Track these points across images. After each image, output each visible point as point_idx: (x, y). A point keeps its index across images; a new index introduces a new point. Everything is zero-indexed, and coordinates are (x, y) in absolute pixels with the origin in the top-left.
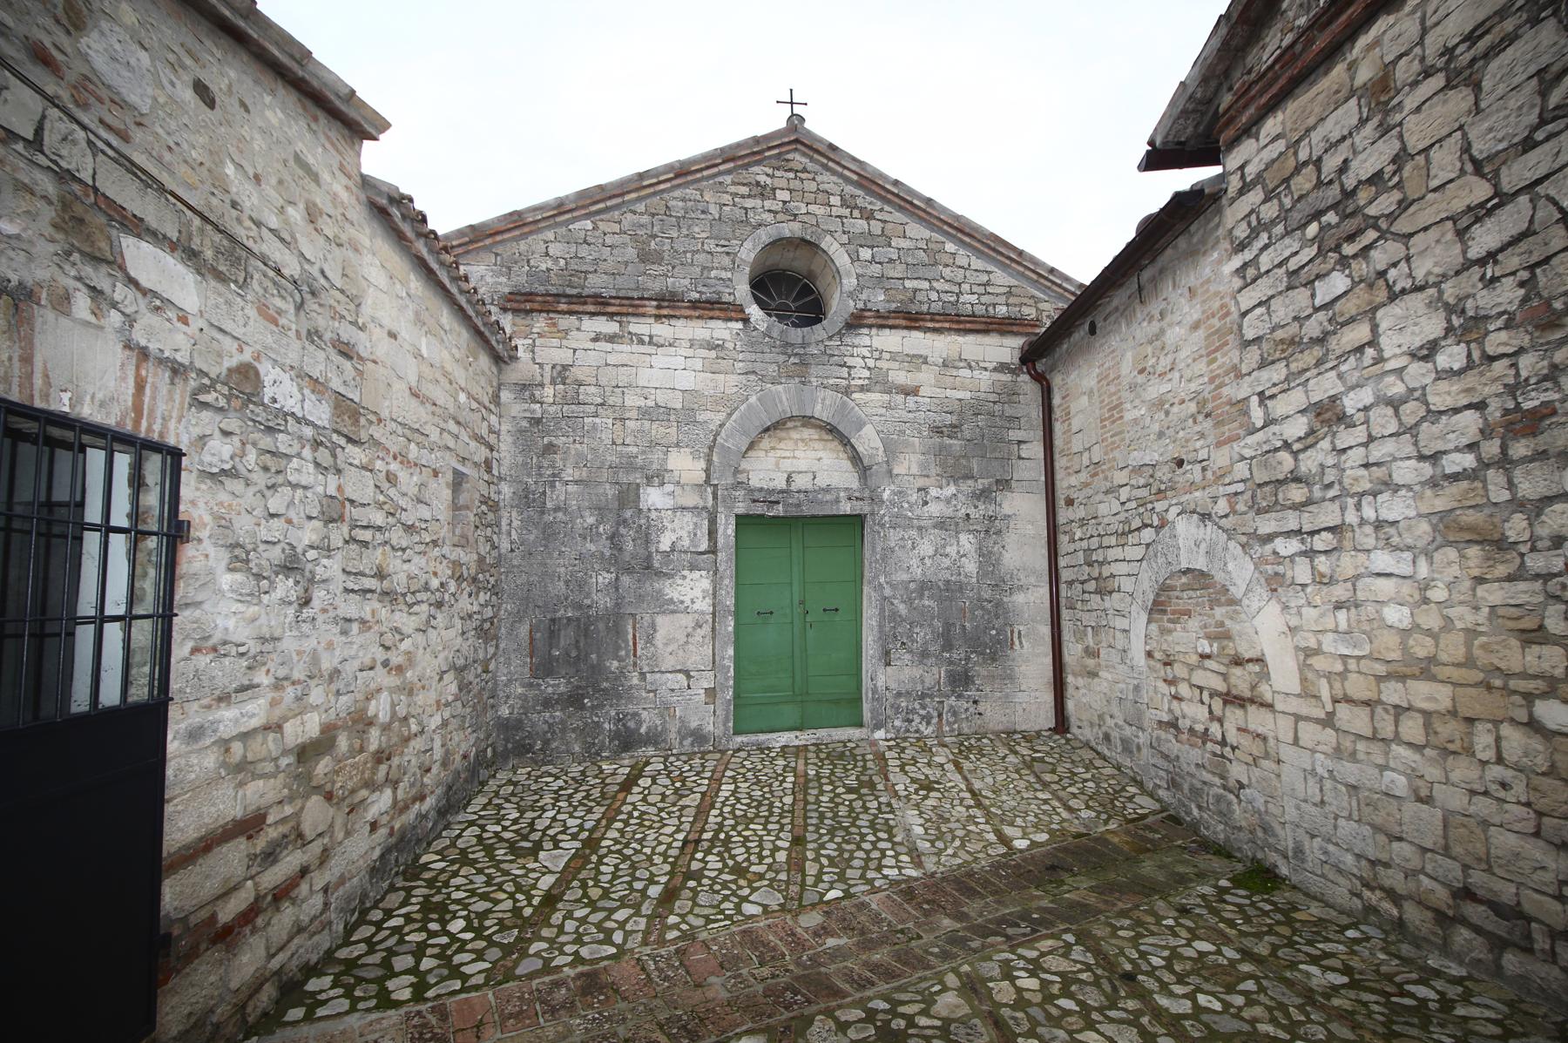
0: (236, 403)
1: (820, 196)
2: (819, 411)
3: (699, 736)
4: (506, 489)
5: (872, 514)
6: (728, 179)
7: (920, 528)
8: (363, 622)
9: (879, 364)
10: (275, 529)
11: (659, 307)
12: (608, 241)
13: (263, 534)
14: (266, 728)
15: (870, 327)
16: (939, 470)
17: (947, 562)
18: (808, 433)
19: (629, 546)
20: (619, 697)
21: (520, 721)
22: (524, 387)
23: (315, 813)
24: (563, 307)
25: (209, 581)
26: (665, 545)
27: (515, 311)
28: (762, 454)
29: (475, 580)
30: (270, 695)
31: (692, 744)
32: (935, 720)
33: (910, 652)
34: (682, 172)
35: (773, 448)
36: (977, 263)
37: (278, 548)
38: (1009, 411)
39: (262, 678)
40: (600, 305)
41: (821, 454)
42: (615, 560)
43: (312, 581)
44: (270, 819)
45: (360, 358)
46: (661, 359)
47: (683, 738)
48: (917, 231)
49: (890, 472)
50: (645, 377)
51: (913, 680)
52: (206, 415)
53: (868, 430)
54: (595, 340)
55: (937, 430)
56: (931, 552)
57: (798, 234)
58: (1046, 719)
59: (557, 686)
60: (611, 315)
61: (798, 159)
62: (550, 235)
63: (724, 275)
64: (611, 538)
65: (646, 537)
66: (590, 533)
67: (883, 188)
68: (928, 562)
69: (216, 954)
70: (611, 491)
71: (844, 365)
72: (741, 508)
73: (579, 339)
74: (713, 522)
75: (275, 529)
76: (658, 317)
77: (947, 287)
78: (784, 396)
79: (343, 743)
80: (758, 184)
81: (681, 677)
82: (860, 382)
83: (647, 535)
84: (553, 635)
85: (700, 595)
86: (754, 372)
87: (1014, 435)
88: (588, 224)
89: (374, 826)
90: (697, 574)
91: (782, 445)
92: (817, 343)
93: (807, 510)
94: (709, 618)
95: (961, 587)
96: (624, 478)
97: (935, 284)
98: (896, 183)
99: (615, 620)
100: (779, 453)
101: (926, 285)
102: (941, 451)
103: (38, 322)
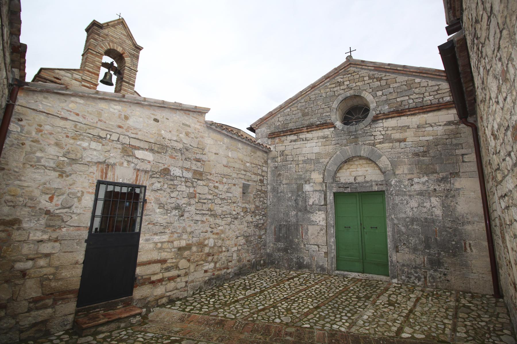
0: (162, 176)
1: (361, 79)
2: (362, 153)
3: (323, 269)
4: (269, 187)
5: (387, 190)
6: (328, 84)
7: (410, 196)
8: (203, 221)
9: (387, 132)
10: (173, 200)
11: (307, 129)
12: (294, 113)
13: (169, 201)
14: (168, 242)
15: (382, 119)
16: (418, 171)
17: (425, 210)
18: (361, 162)
19: (300, 203)
20: (298, 251)
21: (272, 254)
22: (273, 158)
23: (183, 263)
24: (282, 134)
25: (154, 211)
26: (311, 203)
27: (271, 138)
28: (344, 171)
29: (253, 212)
30: (170, 235)
31: (320, 271)
32: (423, 279)
33: (408, 247)
34: (313, 87)
35: (349, 168)
36: (431, 83)
37: (174, 204)
38: (455, 141)
39: (167, 231)
40: (291, 132)
41: (367, 169)
42: (296, 207)
43: (184, 211)
44: (168, 261)
45: (203, 161)
46: (308, 145)
47: (317, 268)
48: (401, 79)
49: (394, 174)
50: (305, 151)
51: (410, 260)
52: (154, 179)
53: (384, 158)
54: (291, 142)
55: (417, 154)
56: (416, 205)
57: (353, 94)
58: (489, 290)
59: (281, 245)
60: (295, 134)
61: (352, 69)
62: (279, 115)
63: (327, 114)
64: (295, 201)
65: (305, 200)
66: (289, 199)
67: (384, 68)
68: (415, 210)
69: (150, 286)
70: (295, 186)
71: (372, 135)
72: (335, 190)
73: (287, 143)
74: (325, 195)
75: (173, 200)
76: (308, 132)
77: (417, 96)
78: (349, 150)
79: (194, 249)
80: (338, 82)
81: (316, 246)
82: (379, 140)
83: (305, 199)
84: (280, 229)
85: (322, 219)
86: (338, 144)
87: (459, 152)
88: (289, 110)
89: (206, 271)
90: (320, 212)
91: (352, 167)
92: (361, 129)
93: (359, 190)
94: (325, 227)
95: (433, 221)
96: (299, 182)
97: (411, 97)
98: (389, 65)
99: (297, 226)
100: (351, 170)
101: (407, 98)
102: (418, 164)
103: (116, 169)
